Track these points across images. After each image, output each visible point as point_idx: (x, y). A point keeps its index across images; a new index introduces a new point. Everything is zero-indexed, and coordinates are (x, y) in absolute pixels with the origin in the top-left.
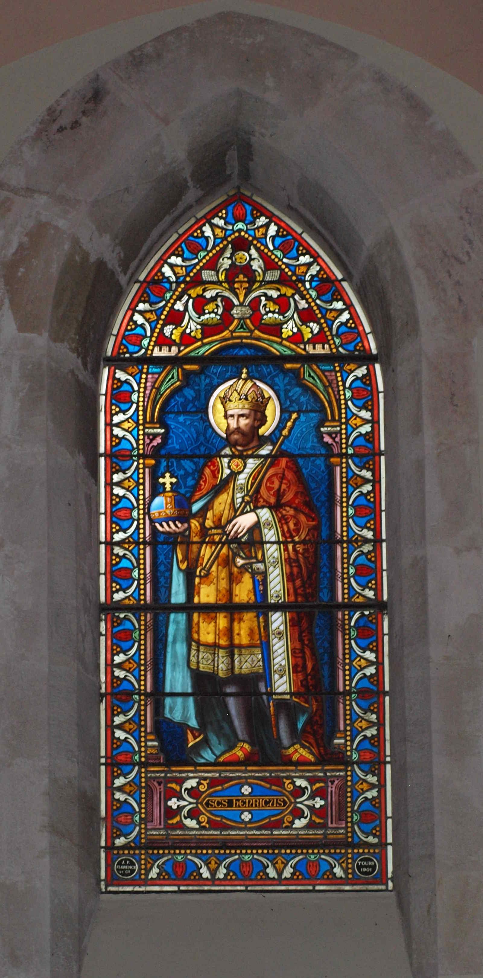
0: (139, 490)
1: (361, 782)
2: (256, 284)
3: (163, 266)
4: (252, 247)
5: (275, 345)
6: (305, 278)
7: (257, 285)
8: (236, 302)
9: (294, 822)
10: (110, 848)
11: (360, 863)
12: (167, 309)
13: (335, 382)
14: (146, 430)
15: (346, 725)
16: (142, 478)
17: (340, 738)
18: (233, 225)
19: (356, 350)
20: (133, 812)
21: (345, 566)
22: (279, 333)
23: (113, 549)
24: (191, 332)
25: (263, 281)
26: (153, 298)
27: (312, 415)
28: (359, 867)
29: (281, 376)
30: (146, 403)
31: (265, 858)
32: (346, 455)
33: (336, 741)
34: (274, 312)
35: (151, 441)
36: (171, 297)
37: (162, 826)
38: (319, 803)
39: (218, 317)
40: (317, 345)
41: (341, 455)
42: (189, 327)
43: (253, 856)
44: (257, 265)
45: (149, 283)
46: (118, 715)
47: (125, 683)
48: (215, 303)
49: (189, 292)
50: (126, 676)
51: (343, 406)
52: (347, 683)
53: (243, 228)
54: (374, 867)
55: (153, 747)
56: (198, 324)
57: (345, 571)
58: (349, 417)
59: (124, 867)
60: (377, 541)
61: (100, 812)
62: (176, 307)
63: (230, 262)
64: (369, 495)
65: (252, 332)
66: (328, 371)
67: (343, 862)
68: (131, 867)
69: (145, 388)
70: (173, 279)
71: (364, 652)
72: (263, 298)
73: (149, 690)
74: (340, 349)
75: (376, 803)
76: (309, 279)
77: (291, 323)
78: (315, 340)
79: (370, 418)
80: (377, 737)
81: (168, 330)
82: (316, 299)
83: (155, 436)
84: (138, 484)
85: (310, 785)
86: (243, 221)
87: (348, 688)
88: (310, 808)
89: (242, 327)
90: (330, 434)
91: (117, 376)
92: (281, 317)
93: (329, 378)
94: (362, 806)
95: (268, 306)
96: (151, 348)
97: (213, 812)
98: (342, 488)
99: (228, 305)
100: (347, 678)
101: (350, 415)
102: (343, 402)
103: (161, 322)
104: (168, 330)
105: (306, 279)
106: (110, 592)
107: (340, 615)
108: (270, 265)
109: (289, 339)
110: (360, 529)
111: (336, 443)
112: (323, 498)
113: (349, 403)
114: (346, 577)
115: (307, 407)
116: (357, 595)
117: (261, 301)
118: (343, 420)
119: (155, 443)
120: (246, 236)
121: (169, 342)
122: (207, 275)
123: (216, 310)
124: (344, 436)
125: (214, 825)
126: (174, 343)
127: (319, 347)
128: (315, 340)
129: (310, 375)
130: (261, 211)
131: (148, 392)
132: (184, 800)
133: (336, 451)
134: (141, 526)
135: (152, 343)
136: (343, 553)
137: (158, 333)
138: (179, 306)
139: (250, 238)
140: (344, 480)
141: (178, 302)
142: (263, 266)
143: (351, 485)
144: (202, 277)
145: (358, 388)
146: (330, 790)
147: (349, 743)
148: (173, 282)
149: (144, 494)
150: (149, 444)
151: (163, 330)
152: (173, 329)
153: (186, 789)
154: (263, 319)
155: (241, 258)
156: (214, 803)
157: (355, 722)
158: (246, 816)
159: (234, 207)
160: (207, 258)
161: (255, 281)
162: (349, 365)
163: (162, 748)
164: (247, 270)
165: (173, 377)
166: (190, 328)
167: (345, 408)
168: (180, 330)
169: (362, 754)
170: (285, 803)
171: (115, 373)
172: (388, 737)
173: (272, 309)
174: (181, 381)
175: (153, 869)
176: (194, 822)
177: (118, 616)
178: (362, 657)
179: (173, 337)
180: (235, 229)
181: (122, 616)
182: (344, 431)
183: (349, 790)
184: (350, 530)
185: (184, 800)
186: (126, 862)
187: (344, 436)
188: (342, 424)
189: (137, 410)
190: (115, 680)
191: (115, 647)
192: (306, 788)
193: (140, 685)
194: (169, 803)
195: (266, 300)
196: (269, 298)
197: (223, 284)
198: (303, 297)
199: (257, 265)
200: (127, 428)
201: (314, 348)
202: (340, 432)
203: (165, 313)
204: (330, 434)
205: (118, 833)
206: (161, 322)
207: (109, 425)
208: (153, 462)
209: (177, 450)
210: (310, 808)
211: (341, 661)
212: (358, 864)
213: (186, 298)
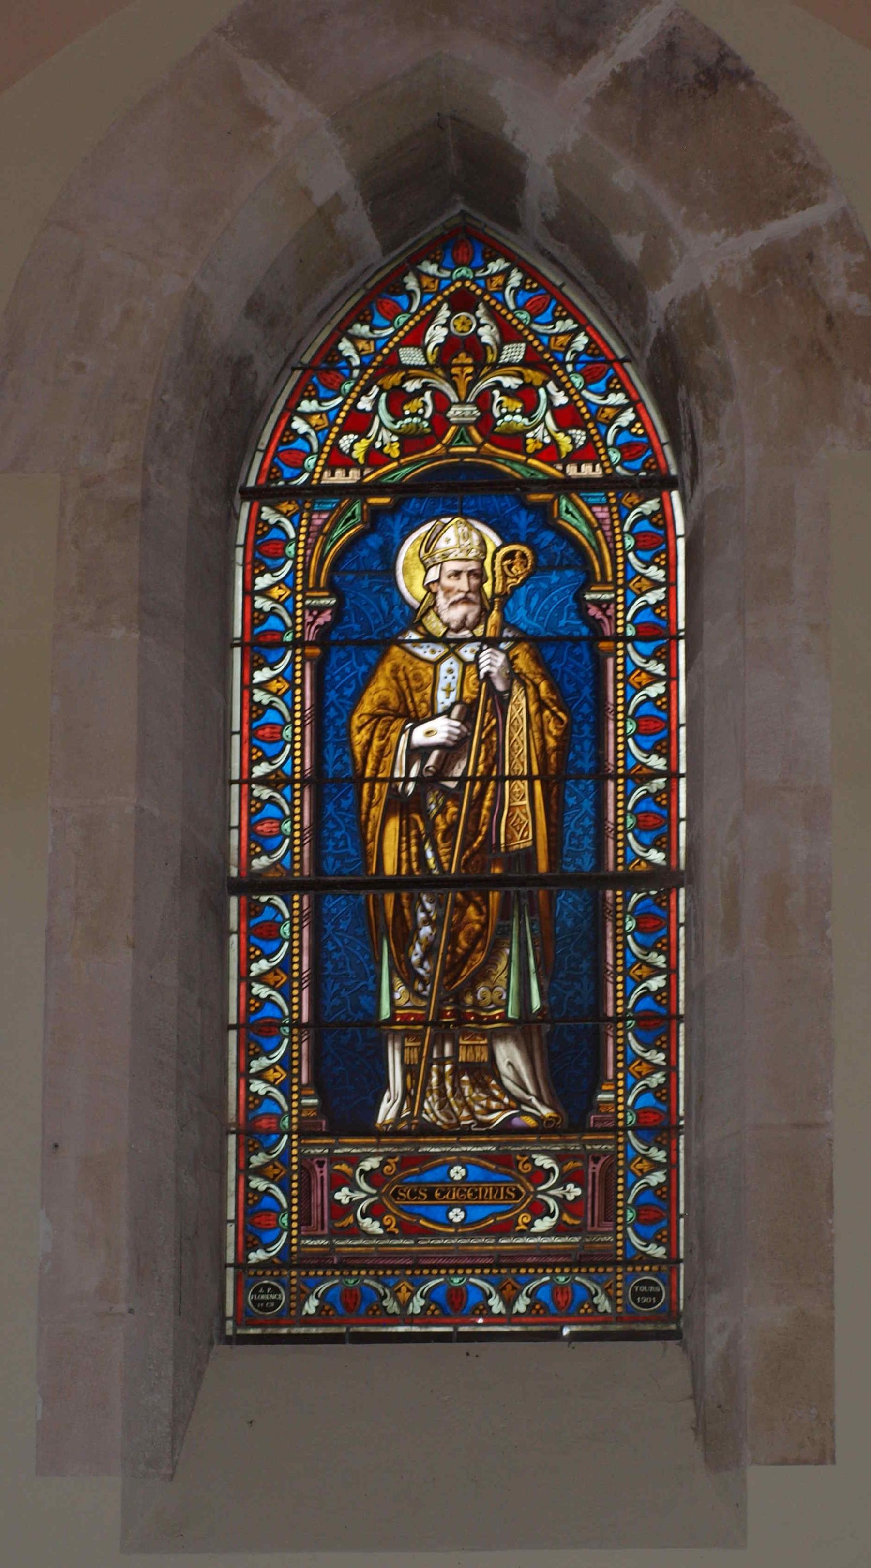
0: (294, 696)
1: (639, 1159)
4: (481, 305)
5: (516, 466)
8: (454, 398)
10: (241, 1265)
11: (637, 1288)
12: (346, 408)
13: (608, 522)
15: (617, 1070)
16: (300, 749)
17: (607, 1092)
18: (452, 271)
19: (643, 468)
21: (620, 812)
23: (254, 602)
24: (383, 446)
26: (323, 393)
27: (569, 573)
28: (635, 1294)
29: (523, 513)
30: (308, 558)
32: (626, 639)
33: (601, 1097)
34: (514, 414)
35: (316, 618)
36: (352, 390)
37: (326, 1231)
40: (583, 466)
41: (617, 638)
42: (380, 438)
43: (468, 1280)
44: (487, 334)
47: (267, 1102)
52: (620, 1002)
54: (658, 1295)
55: (312, 1106)
56: (394, 433)
57: (621, 820)
58: (630, 576)
60: (672, 775)
61: (227, 1110)
62: (360, 406)
63: (445, 332)
67: (610, 1287)
68: (273, 1297)
70: (356, 361)
71: (647, 568)
72: (496, 393)
75: (662, 1042)
77: (540, 430)
78: (578, 456)
80: (665, 793)
81: (345, 442)
82: (582, 389)
83: (321, 609)
84: (293, 686)
85: (557, 1164)
86: (468, 265)
87: (620, 1010)
88: (561, 1201)
91: (264, 516)
92: (526, 421)
94: (641, 709)
95: (504, 405)
97: (405, 1208)
99: (441, 403)
100: (620, 796)
103: (336, 429)
104: (345, 442)
107: (609, 894)
109: (536, 455)
111: (609, 617)
112: (587, 822)
114: (620, 934)
115: (561, 561)
116: (638, 578)
117: (493, 397)
118: (620, 582)
119: (320, 621)
120: (473, 288)
121: (347, 462)
122: (410, 356)
123: (421, 411)
125: (408, 1229)
126: (355, 464)
128: (578, 456)
129: (567, 511)
130: (495, 251)
132: (360, 1190)
133: (608, 631)
135: (321, 463)
136: (617, 793)
137: (331, 446)
138: (365, 404)
139: (479, 292)
141: (364, 398)
143: (632, 1074)
146: (590, 1171)
147: (621, 1100)
149: (302, 703)
150: (312, 623)
155: (463, 324)
156: (406, 1193)
157: (631, 1065)
158: (456, 1215)
160: (412, 323)
161: (485, 364)
163: (323, 1109)
164: (473, 344)
166: (382, 441)
168: (365, 443)
169: (643, 723)
170: (518, 1194)
171: (261, 512)
172: (682, 941)
173: (511, 409)
176: (377, 1224)
177: (258, 900)
178: (643, 576)
179: (355, 455)
180: (454, 277)
181: (264, 899)
183: (621, 1173)
184: (629, 568)
185: (360, 1190)
186: (266, 1290)
188: (618, 587)
189: (294, 569)
190: (250, 1195)
194: (338, 1196)
196: (506, 392)
198: (561, 387)
199: (487, 334)
200: (277, 597)
202: (614, 601)
203: (343, 414)
204: (598, 603)
205: (257, 1050)
206: (336, 429)
207: (250, 593)
208: (317, 651)
209: (356, 632)
212: (633, 1289)
213: (375, 390)
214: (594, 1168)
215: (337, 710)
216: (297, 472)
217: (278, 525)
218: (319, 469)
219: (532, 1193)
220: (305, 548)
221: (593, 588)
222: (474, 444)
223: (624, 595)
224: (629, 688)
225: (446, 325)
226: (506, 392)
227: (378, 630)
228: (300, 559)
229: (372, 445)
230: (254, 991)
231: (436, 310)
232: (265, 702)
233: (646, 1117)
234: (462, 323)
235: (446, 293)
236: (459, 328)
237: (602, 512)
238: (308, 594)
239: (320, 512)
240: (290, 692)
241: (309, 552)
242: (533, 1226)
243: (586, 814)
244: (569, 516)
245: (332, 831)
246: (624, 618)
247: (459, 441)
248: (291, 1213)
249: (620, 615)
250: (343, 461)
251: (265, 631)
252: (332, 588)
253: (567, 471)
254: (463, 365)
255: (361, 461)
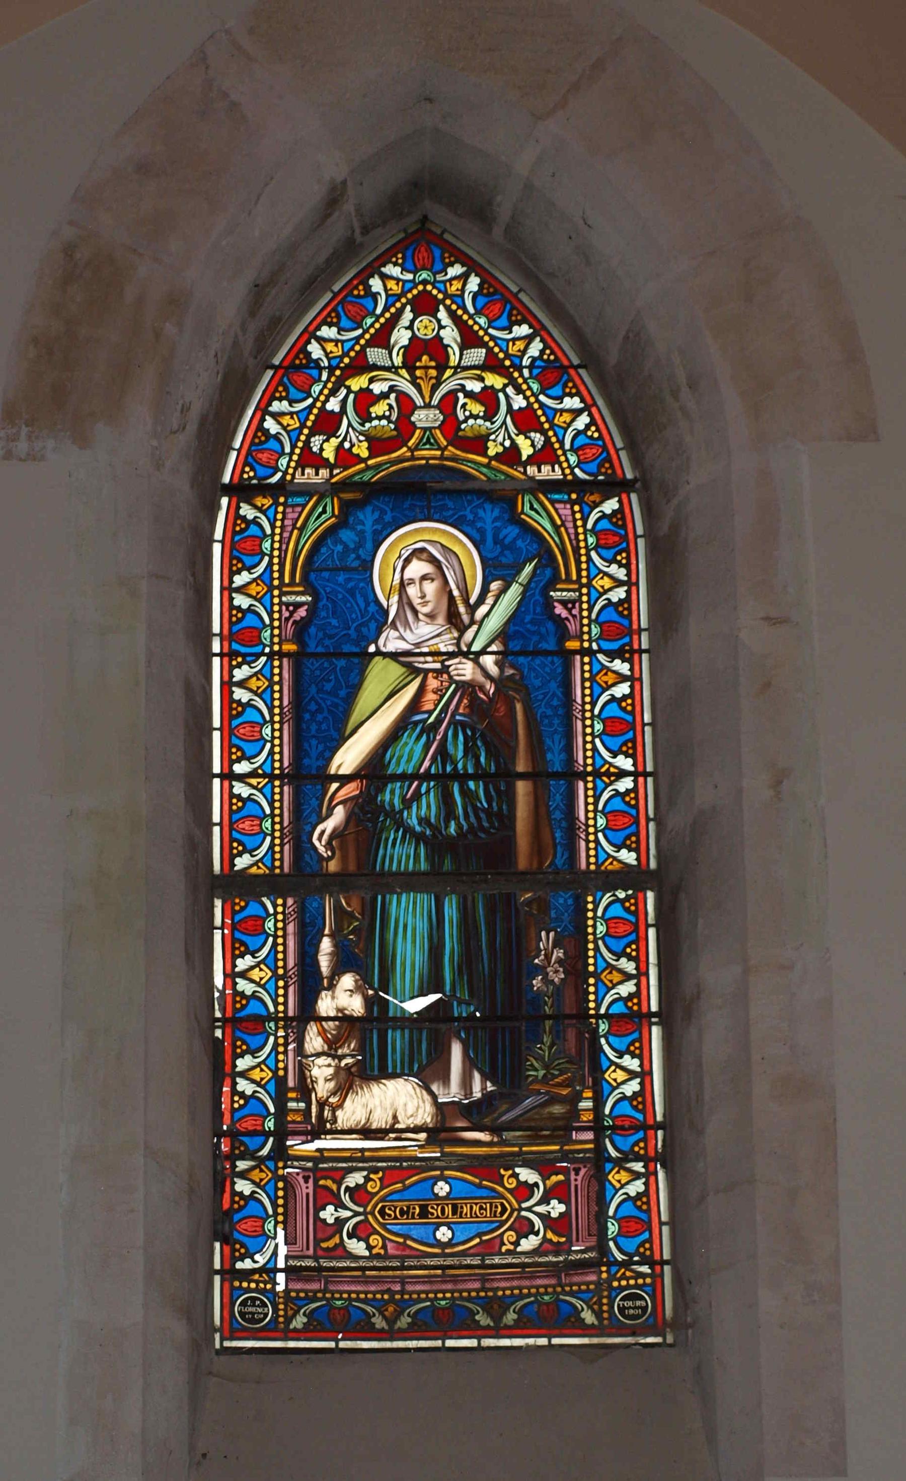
2: (448, 370)
3: (310, 343)
6: (521, 361)
7: (449, 373)
8: (419, 401)
9: (500, 668)
11: (621, 1303)
12: (315, 411)
13: (570, 518)
14: (284, 599)
20: (264, 1216)
22: (483, 452)
24: (352, 445)
25: (458, 366)
31: (473, 1303)
34: (476, 417)
35: (292, 614)
38: (556, 1208)
39: (392, 426)
40: (543, 467)
44: (450, 335)
45: (287, 368)
46: (242, 1056)
48: (387, 401)
49: (347, 383)
50: (255, 1092)
51: (584, 559)
53: (429, 278)
59: (251, 1309)
63: (409, 334)
64: (625, 701)
65: (443, 449)
66: (560, 502)
69: (282, 527)
72: (461, 395)
73: (291, 1013)
74: (577, 471)
76: (528, 364)
78: (537, 459)
79: (626, 578)
81: (316, 442)
83: (298, 606)
88: (542, 1217)
89: (428, 442)
90: (564, 603)
91: (242, 512)
92: (488, 424)
93: (561, 512)
95: (468, 407)
96: (291, 471)
98: (583, 688)
99: (406, 405)
101: (594, 572)
102: (583, 551)
103: (306, 431)
105: (524, 364)
106: (229, 858)
108: (469, 339)
109: (498, 457)
110: (607, 564)
111: (574, 616)
113: (593, 554)
117: (457, 399)
118: (584, 581)
122: (375, 355)
123: (387, 413)
124: (585, 606)
127: (546, 469)
128: (537, 459)
129: (532, 508)
131: (286, 535)
134: (277, 749)
135: (293, 464)
138: (333, 405)
140: (587, 675)
141: (332, 399)
142: (459, 340)
144: (367, 359)
145: (605, 531)
146: (573, 1183)
148: (325, 368)
150: (287, 619)
151: (310, 442)
152: (324, 441)
153: (348, 1189)
154: (461, 430)
159: (415, 249)
160: (377, 326)
162: (592, 494)
164: (436, 347)
165: (324, 511)
166: (351, 441)
167: (587, 562)
168: (334, 442)
174: (336, 517)
175: (298, 1317)
179: (325, 454)
182: (585, 598)
187: (585, 606)
188: (582, 586)
189: (270, 564)
191: (238, 999)
192: (536, 1185)
193: (276, 1004)
195: (465, 397)
196: (469, 395)
197: (400, 370)
198: (519, 391)
201: (539, 471)
204: (564, 603)
206: (306, 431)
210: (542, 1217)
211: (580, 708)
212: (619, 1305)
213: (343, 392)
214: (576, 1180)
215: (317, 703)
216: (270, 471)
217: (255, 521)
218: (291, 471)
219: (516, 1210)
220: (280, 542)
221: (558, 586)
222: (439, 448)
223: (588, 594)
224: (595, 686)
225: (410, 327)
226: (469, 395)
227: (355, 625)
228: (276, 553)
229: (341, 444)
230: (236, 603)
231: (400, 312)
232: (248, 993)
233: (627, 1227)
234: (425, 327)
235: (410, 296)
236: (423, 331)
237: (565, 508)
238: (285, 589)
239: (293, 506)
240: (269, 594)
241: (284, 547)
242: (519, 1245)
243: (554, 695)
244: (533, 513)
245: (313, 714)
246: (589, 617)
247: (425, 444)
248: (273, 628)
249: (585, 613)
250: (313, 460)
251: (246, 917)
252: (309, 586)
253: (528, 473)
254: (426, 368)
255: (332, 460)
